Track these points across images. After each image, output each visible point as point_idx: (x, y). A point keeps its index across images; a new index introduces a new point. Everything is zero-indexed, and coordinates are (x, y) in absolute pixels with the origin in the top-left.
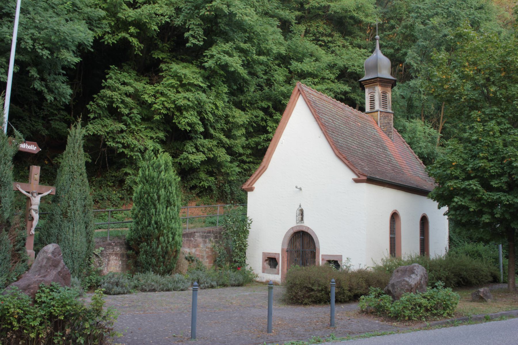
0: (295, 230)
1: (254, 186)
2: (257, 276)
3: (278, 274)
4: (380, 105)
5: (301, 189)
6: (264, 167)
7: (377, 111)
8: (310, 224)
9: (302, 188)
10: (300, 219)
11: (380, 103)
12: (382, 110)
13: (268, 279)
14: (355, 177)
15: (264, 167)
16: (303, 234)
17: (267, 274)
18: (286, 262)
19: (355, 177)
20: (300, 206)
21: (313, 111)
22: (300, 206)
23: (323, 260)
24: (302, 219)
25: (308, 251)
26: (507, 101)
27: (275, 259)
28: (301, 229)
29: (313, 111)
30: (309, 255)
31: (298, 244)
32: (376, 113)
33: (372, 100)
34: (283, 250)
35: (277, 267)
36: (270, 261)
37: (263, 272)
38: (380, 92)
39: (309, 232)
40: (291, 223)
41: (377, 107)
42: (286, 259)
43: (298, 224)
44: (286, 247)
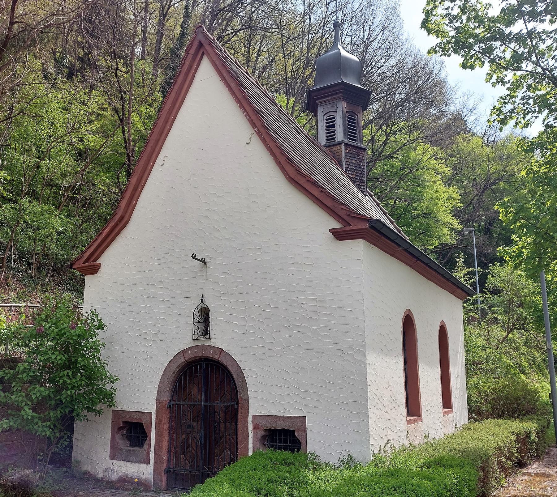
0: (189, 356)
1: (99, 261)
2: (101, 326)
3: (147, 462)
4: (345, 134)
5: (203, 261)
6: (122, 218)
7: (340, 143)
8: (223, 338)
9: (207, 260)
10: (201, 330)
11: (344, 130)
12: (347, 141)
13: (122, 474)
14: (336, 225)
15: (122, 218)
16: (207, 365)
17: (122, 463)
18: (166, 433)
19: (336, 225)
20: (202, 301)
21: (233, 85)
22: (202, 301)
23: (255, 428)
24: (206, 331)
25: (219, 405)
26: (524, 183)
27: (141, 425)
28: (203, 353)
29: (233, 85)
30: (222, 415)
31: (196, 391)
32: (338, 148)
33: (331, 125)
34: (159, 402)
35: (145, 446)
36: (130, 431)
37: (113, 457)
38: (345, 110)
39: (222, 359)
40: (183, 338)
41: (340, 136)
42: (166, 426)
43: (197, 344)
44: (166, 398)
